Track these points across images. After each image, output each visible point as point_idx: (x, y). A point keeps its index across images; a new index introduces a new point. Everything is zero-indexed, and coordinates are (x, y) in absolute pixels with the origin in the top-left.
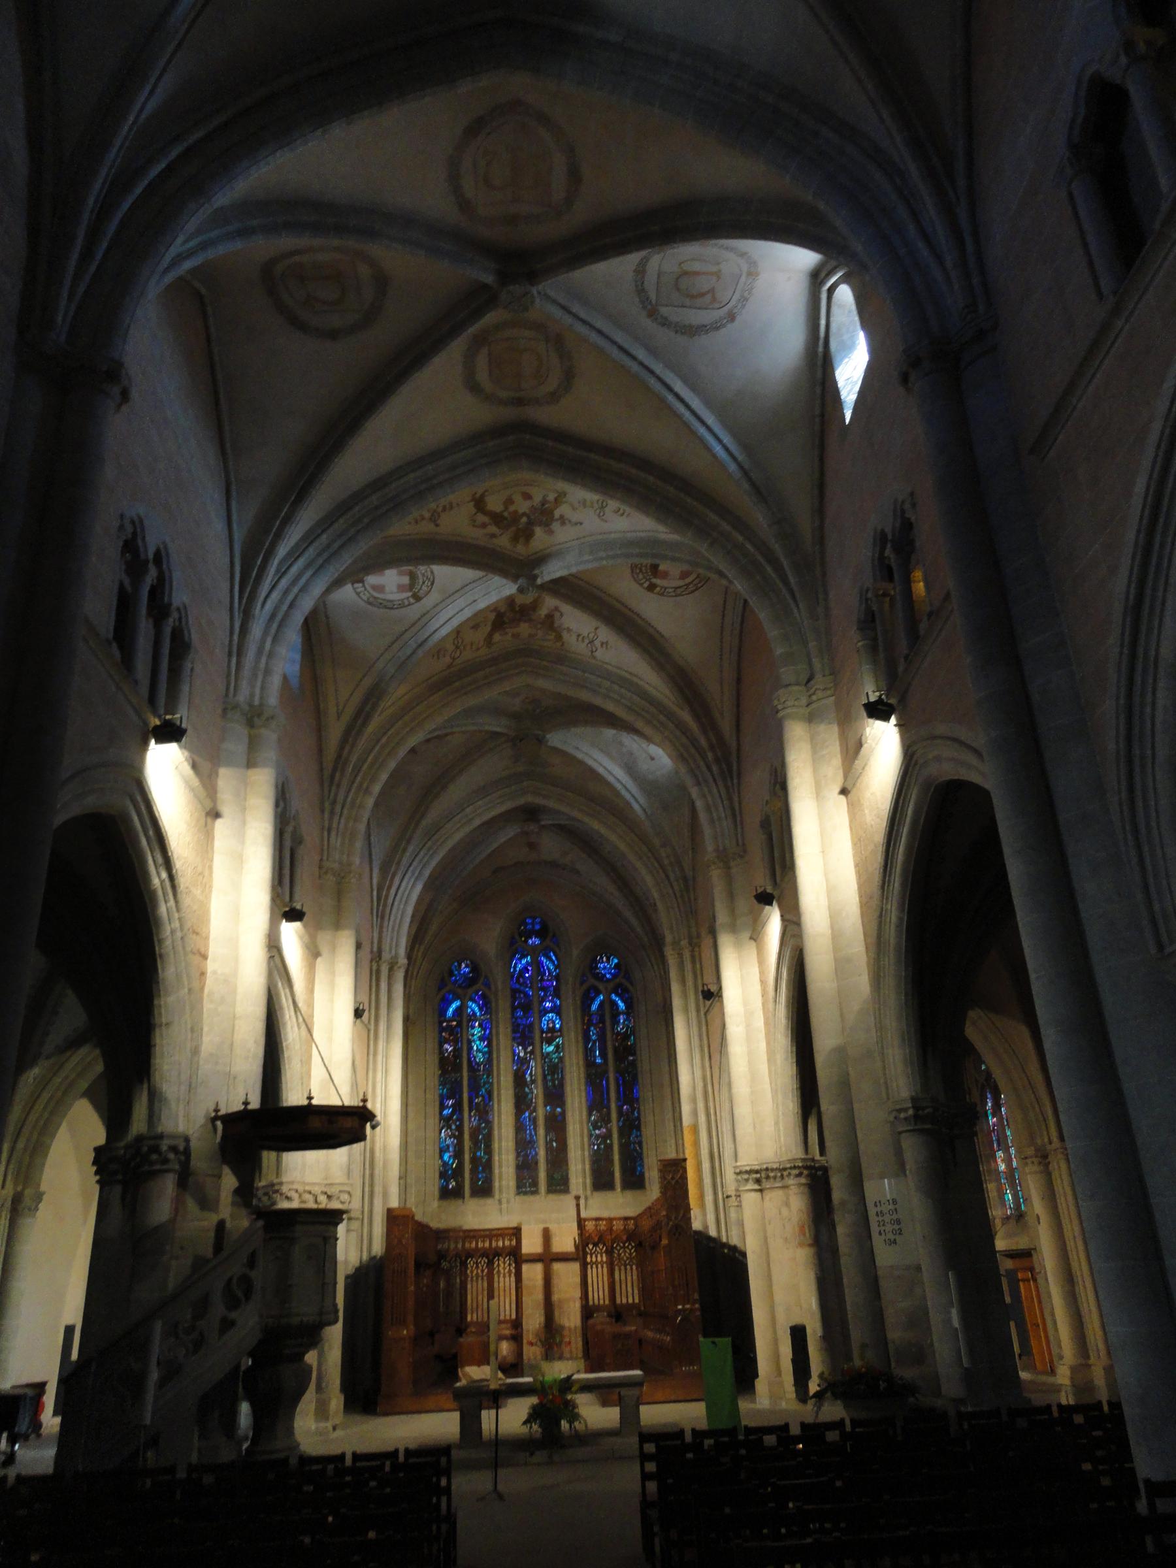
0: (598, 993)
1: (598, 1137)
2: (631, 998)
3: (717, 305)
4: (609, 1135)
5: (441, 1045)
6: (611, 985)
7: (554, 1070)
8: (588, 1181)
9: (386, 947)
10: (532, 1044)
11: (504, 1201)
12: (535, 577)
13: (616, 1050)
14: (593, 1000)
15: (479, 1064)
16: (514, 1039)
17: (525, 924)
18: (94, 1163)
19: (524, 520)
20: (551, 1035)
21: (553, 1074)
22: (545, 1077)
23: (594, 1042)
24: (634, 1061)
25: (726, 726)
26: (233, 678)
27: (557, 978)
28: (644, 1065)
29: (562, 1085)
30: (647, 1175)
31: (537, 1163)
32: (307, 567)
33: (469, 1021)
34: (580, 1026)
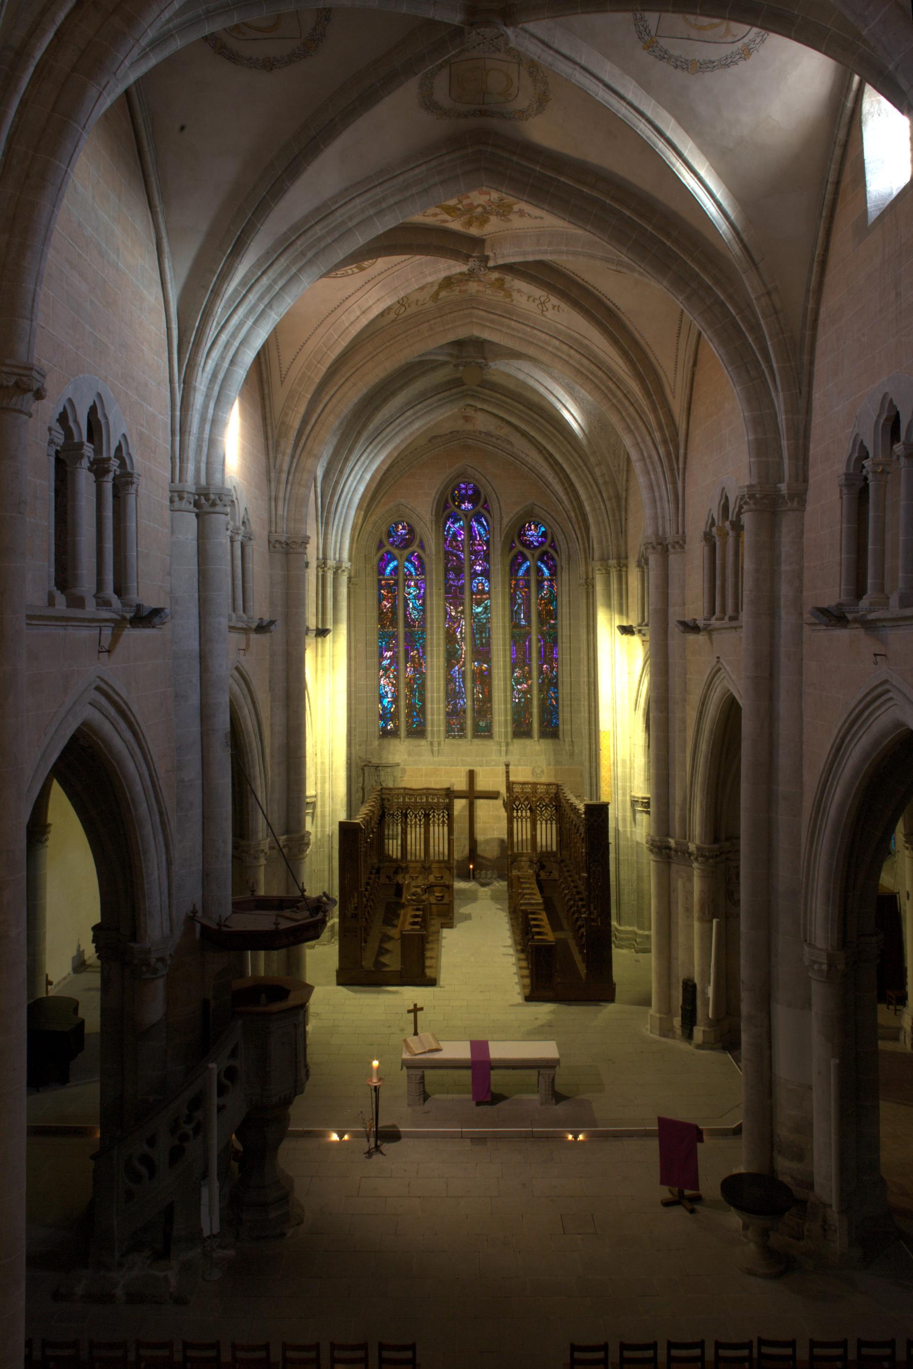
0: (525, 559)
1: (519, 691)
2: (555, 566)
3: (730, 39)
4: (529, 690)
5: (380, 602)
6: (537, 553)
7: (481, 629)
8: (509, 729)
9: (331, 554)
10: (463, 604)
11: (436, 744)
12: (486, 259)
13: (539, 614)
14: (520, 565)
15: (413, 620)
16: (446, 599)
17: (460, 489)
18: (93, 942)
19: (480, 210)
20: (479, 597)
21: (481, 633)
22: (473, 635)
23: (520, 605)
24: (555, 624)
25: (677, 405)
26: (178, 460)
27: (487, 543)
28: (564, 633)
29: (488, 644)
30: (561, 727)
31: (464, 712)
32: (247, 316)
33: (405, 580)
34: (507, 590)
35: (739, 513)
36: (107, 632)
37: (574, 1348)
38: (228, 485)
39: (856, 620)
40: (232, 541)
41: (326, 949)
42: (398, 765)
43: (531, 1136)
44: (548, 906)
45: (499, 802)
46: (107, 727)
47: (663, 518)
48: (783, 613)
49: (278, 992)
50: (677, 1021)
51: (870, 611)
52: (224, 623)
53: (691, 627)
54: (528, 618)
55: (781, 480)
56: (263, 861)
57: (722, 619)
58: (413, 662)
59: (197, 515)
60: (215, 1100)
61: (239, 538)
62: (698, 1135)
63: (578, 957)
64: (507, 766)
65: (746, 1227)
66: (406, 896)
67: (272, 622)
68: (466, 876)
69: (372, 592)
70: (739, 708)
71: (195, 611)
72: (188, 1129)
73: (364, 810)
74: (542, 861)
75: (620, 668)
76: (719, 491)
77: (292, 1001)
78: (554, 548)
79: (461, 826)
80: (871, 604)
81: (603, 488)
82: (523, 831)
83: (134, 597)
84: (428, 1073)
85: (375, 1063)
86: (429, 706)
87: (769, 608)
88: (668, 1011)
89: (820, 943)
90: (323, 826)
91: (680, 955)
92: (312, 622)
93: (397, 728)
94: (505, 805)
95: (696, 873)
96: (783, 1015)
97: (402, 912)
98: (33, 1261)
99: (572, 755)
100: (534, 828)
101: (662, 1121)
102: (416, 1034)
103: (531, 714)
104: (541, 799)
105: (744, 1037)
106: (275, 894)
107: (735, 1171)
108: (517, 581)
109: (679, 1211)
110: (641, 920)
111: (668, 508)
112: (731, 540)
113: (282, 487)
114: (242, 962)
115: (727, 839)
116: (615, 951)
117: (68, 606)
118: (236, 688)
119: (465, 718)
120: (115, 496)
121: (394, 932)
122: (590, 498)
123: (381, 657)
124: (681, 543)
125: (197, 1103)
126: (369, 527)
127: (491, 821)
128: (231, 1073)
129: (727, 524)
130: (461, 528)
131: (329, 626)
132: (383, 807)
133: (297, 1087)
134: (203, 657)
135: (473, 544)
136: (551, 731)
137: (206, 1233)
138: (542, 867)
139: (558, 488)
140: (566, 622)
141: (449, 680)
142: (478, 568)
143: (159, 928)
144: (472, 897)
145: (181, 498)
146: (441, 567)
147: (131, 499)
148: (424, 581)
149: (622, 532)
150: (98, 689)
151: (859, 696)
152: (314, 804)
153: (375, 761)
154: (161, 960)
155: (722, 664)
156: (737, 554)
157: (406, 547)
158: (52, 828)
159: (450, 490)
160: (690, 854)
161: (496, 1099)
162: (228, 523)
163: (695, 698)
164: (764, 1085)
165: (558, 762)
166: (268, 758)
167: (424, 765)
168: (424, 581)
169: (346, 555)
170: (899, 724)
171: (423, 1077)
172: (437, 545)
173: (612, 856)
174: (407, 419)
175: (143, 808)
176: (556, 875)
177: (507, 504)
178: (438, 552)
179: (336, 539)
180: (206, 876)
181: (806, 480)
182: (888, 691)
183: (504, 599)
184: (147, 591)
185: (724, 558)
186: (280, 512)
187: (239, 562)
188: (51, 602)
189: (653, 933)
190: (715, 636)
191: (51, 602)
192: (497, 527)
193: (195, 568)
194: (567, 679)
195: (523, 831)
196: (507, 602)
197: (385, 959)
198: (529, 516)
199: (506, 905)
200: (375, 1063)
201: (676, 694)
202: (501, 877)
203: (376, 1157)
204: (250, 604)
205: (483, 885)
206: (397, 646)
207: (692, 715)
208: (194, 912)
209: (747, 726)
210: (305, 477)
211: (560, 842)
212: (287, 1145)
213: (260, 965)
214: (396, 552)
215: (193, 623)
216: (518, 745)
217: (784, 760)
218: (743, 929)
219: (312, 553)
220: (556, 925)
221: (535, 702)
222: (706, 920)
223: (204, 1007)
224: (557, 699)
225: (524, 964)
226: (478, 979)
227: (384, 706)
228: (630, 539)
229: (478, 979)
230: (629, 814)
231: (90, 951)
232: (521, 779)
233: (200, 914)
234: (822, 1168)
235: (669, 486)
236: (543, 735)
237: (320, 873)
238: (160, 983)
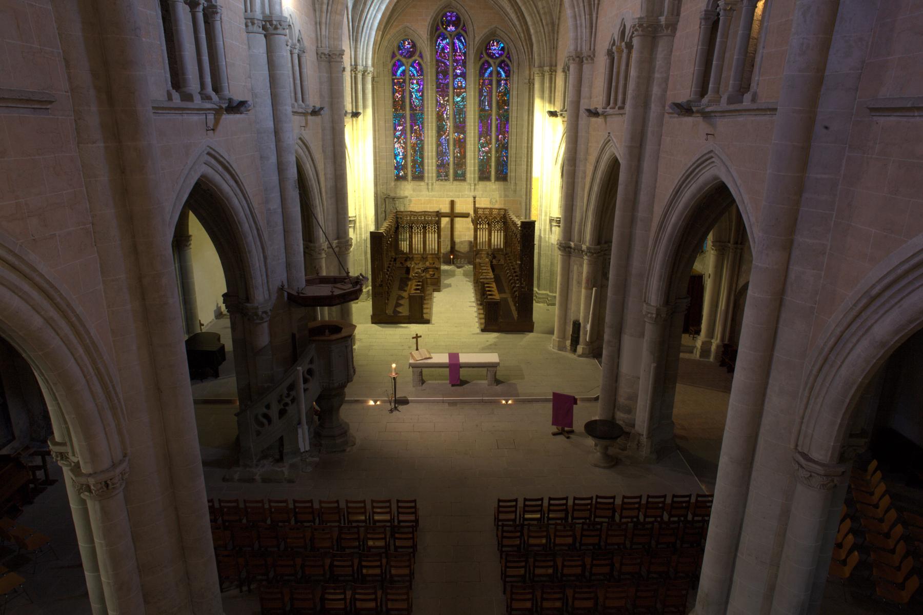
0: (490, 65)
1: (483, 152)
4: (490, 151)
6: (498, 61)
7: (460, 112)
9: (360, 62)
10: (448, 96)
13: (498, 102)
14: (486, 69)
22: (455, 116)
27: (465, 54)
28: (513, 115)
29: (464, 122)
35: (631, 37)
36: (211, 117)
37: (499, 501)
38: (286, 14)
39: (698, 112)
40: (292, 54)
41: (365, 304)
42: (407, 197)
43: (483, 401)
44: (497, 279)
45: (469, 219)
46: (217, 178)
47: (582, 39)
48: (653, 106)
49: (336, 329)
50: (568, 343)
51: (708, 106)
52: (289, 109)
53: (593, 113)
54: (490, 105)
55: (661, 14)
56: (324, 255)
57: (614, 108)
58: (416, 133)
59: (265, 36)
60: (302, 386)
61: (296, 51)
62: (575, 401)
63: (513, 308)
64: (474, 198)
65: (596, 445)
66: (412, 274)
67: (322, 109)
68: (449, 262)
69: (389, 87)
70: (619, 164)
71: (269, 102)
72: (288, 400)
73: (386, 225)
74: (494, 254)
75: (547, 137)
76: (620, 21)
77: (344, 333)
78: (509, 58)
79: (445, 233)
80: (709, 101)
81: (543, 17)
82: (483, 236)
83: (227, 93)
84: (424, 370)
85: (394, 366)
86: (426, 161)
87: (644, 102)
88: (563, 337)
89: (653, 303)
90: (361, 234)
91: (573, 307)
92: (349, 107)
93: (406, 174)
94: (473, 221)
95: (585, 262)
96: (628, 341)
97: (410, 283)
98: (205, 464)
99: (515, 191)
100: (490, 235)
101: (555, 394)
102: (417, 349)
103: (490, 166)
104: (495, 218)
105: (604, 352)
106: (332, 274)
107: (593, 419)
108: (484, 80)
109: (561, 438)
110: (551, 286)
111: (585, 32)
112: (624, 55)
113: (324, 15)
114: (315, 312)
115: (606, 243)
116: (535, 305)
117: (182, 100)
118: (300, 151)
119: (448, 168)
120: (206, 22)
121: (405, 294)
122: (534, 24)
123: (395, 129)
124: (592, 57)
125: (291, 387)
126: (385, 43)
127: (464, 231)
128: (310, 372)
129: (623, 44)
130: (448, 44)
131: (360, 110)
132: (397, 222)
133: (349, 379)
134: (277, 132)
135: (455, 55)
136: (502, 176)
137: (302, 450)
138: (494, 257)
139: (513, 16)
140: (515, 108)
141: (439, 145)
142: (458, 71)
143: (262, 295)
144: (451, 274)
145: (253, 24)
146: (434, 70)
147: (218, 25)
148: (423, 80)
149: (554, 48)
150: (209, 154)
151: (694, 160)
152: (354, 221)
153: (392, 195)
154: (265, 312)
155: (611, 137)
156: (627, 65)
157: (411, 56)
158: (193, 238)
159: (440, 17)
160: (583, 251)
161: (463, 383)
162: (287, 41)
163: (592, 159)
164: (614, 376)
165: (506, 196)
166: (324, 194)
167: (422, 197)
168: (423, 80)
169: (370, 62)
170: (716, 178)
171: (421, 372)
172: (431, 55)
173: (536, 251)
174: (371, 29)
175: (246, 226)
176: (502, 262)
177: (478, 28)
178: (432, 60)
179: (363, 52)
180: (289, 266)
181: (678, 14)
182: (712, 157)
183: (475, 92)
184: (236, 89)
185: (619, 67)
186: (323, 33)
187: (297, 68)
188: (170, 98)
189: (557, 295)
190: (608, 119)
191: (170, 98)
192: (472, 43)
193: (266, 72)
194: (513, 144)
195: (483, 236)
196: (477, 94)
197: (399, 309)
198: (493, 36)
199: (472, 279)
200: (394, 366)
201: (581, 155)
202: (469, 263)
203: (395, 413)
204: (306, 96)
205: (459, 267)
206: (405, 123)
207: (590, 169)
208: (283, 286)
209: (623, 177)
210: (339, 7)
211: (506, 243)
212: (344, 408)
213: (325, 314)
214: (404, 60)
215: (268, 110)
216: (482, 185)
217: (643, 197)
218: (609, 294)
219: (347, 61)
220: (501, 290)
221: (493, 159)
222: (589, 288)
223: (292, 338)
224: (507, 157)
225: (482, 311)
226: (454, 317)
227: (398, 162)
228: (559, 53)
229: (454, 317)
230: (548, 227)
231: (223, 308)
232: (483, 206)
233: (286, 286)
234: (641, 418)
235: (587, 17)
236: (498, 179)
237: (359, 261)
238: (266, 325)
